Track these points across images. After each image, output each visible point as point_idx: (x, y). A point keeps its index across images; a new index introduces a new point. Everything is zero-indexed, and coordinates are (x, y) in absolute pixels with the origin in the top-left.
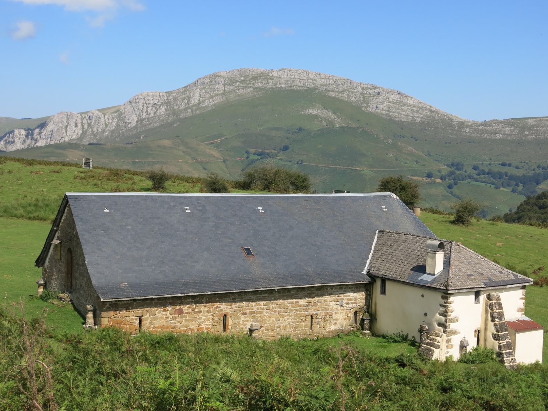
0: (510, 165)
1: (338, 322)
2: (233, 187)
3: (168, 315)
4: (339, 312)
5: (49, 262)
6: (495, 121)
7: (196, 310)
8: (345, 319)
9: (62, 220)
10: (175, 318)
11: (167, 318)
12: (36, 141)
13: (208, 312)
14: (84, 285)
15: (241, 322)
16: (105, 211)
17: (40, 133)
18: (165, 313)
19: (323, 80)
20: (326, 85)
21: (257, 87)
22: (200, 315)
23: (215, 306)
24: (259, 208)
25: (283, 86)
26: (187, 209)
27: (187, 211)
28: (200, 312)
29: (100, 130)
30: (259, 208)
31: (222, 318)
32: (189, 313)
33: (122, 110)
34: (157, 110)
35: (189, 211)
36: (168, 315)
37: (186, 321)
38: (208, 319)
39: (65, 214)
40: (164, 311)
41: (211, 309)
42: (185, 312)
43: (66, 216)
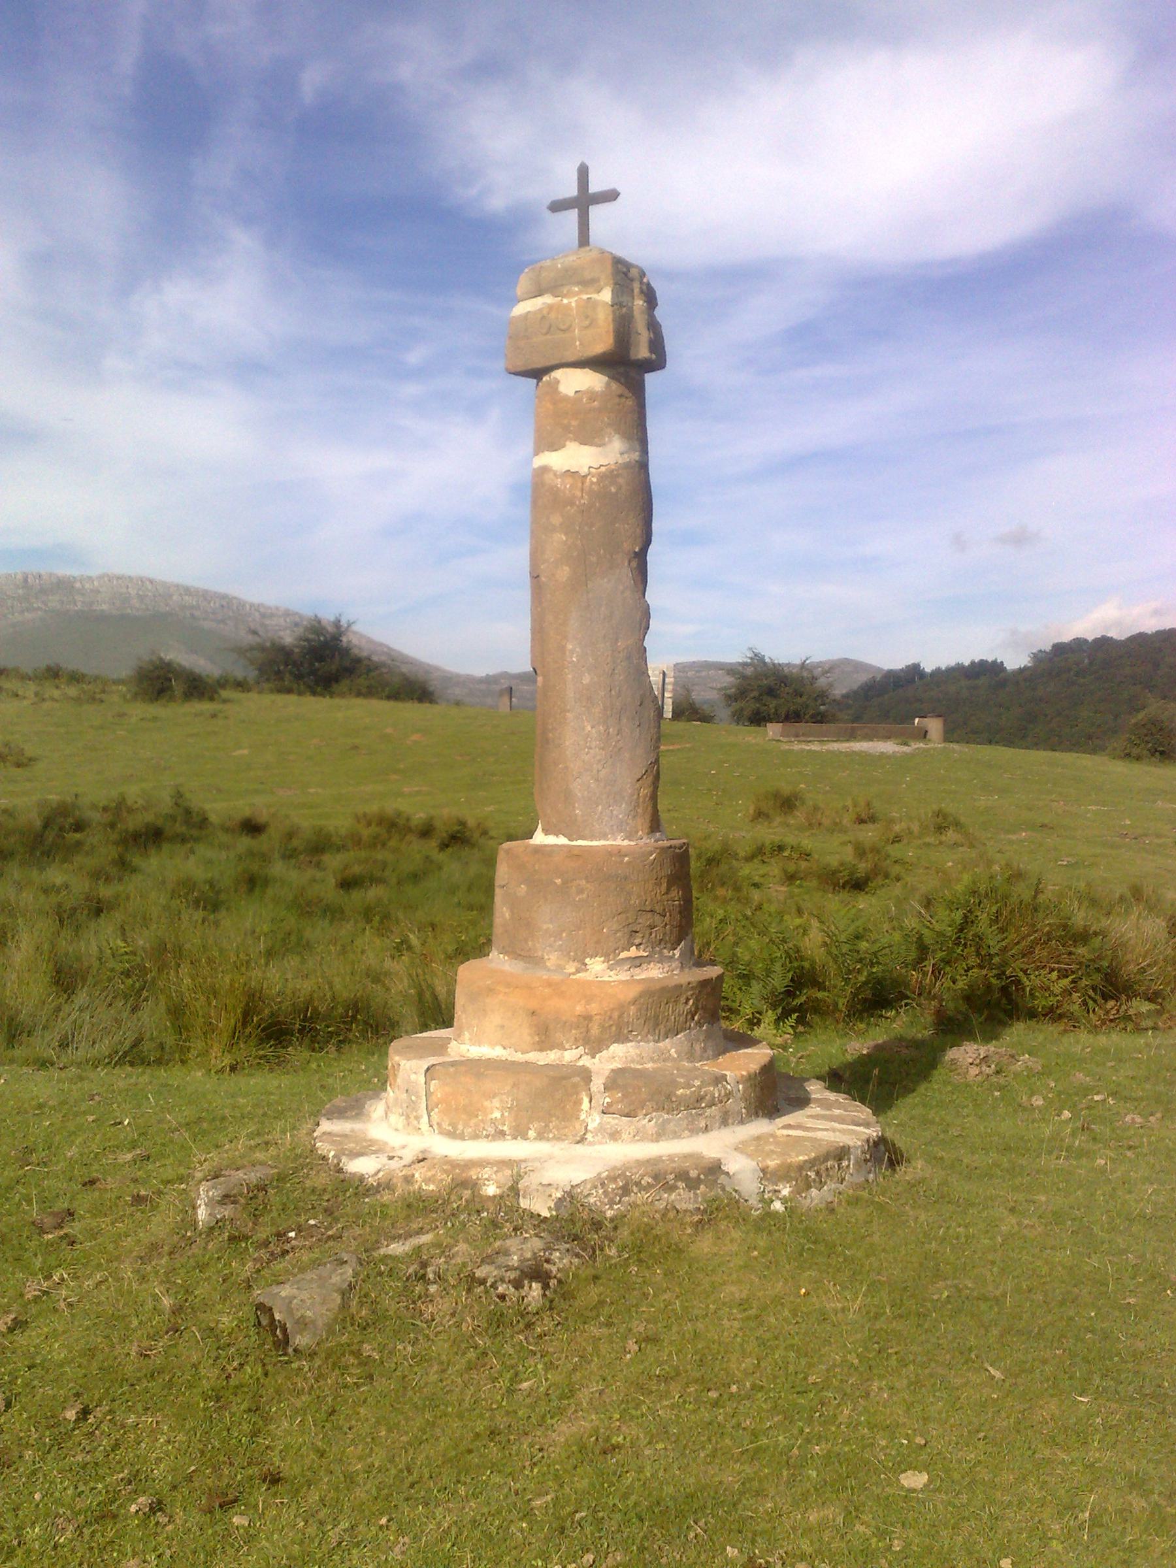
20: (192, 607)
25: (104, 607)
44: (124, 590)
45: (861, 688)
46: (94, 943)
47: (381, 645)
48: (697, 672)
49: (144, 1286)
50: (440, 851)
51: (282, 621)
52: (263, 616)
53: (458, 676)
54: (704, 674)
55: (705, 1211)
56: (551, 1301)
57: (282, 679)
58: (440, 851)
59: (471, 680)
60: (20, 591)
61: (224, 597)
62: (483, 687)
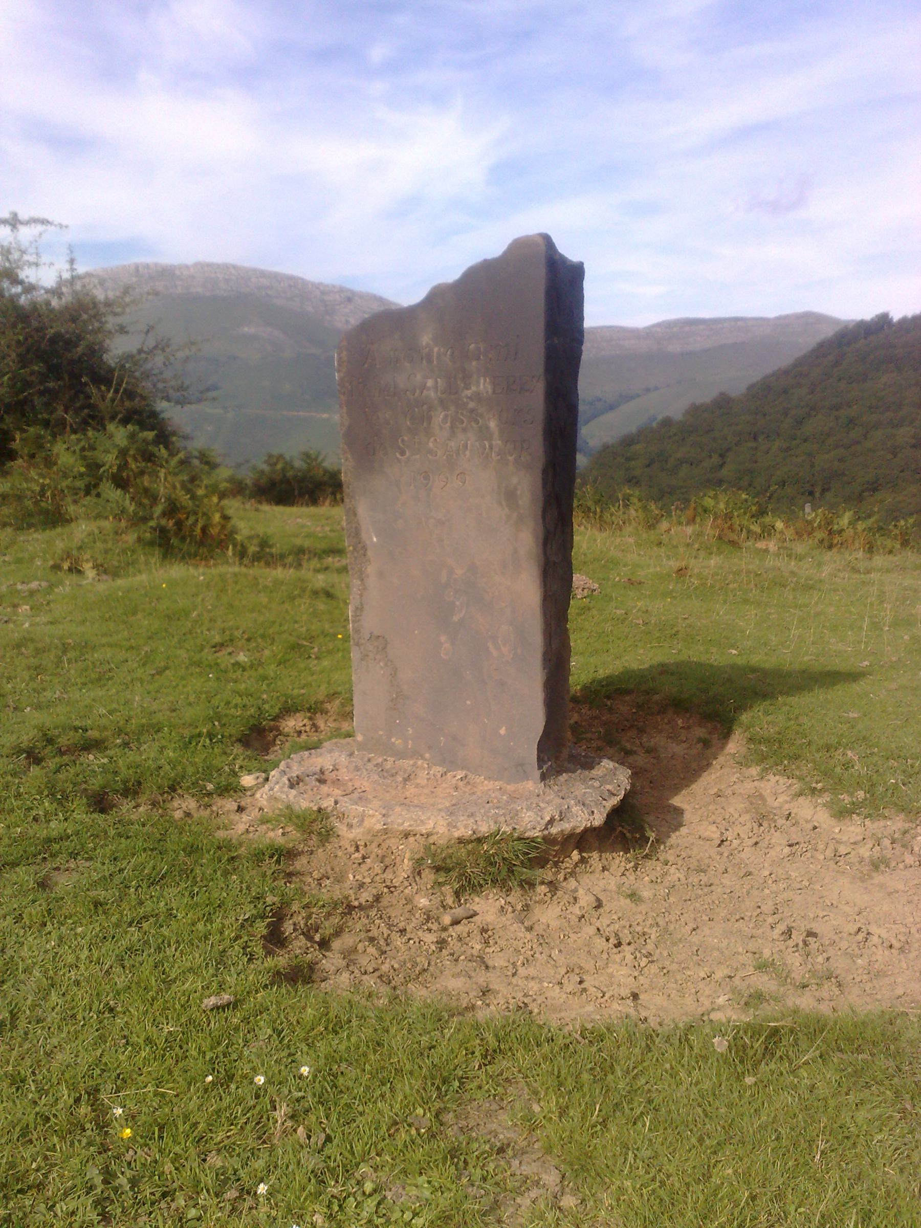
25: (200, 290)
52: (323, 293)
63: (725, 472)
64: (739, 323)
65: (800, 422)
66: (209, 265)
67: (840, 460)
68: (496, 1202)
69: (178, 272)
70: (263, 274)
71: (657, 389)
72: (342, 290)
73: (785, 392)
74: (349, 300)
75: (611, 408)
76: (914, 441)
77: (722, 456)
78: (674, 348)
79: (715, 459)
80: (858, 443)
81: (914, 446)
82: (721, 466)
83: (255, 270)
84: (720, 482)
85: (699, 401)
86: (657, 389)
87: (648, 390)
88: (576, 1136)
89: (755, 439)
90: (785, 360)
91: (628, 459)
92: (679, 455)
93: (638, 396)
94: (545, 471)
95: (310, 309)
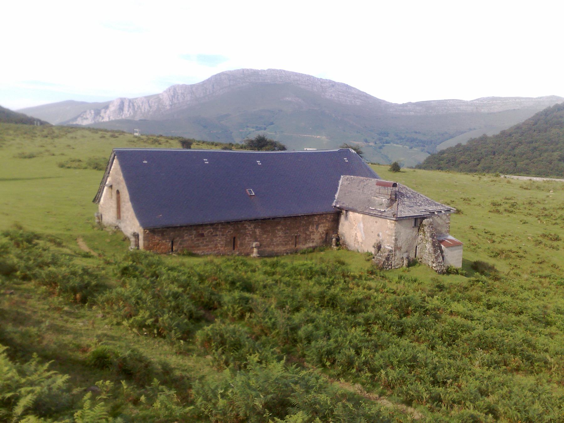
0: (419, 133)
1: (315, 241)
2: (42, 299)
3: (193, 238)
4: (315, 234)
5: (103, 200)
6: (410, 103)
7: (214, 234)
8: (319, 239)
9: (112, 169)
10: (198, 240)
11: (192, 240)
12: (103, 118)
13: (223, 235)
14: (129, 217)
15: (246, 242)
16: (144, 162)
17: (105, 112)
18: (191, 236)
19: (296, 77)
20: (297, 80)
21: (66, 412)
22: (217, 238)
23: (227, 231)
24: (258, 162)
25: (269, 81)
26: (206, 161)
27: (205, 163)
28: (217, 235)
29: (146, 110)
30: (258, 162)
31: (232, 240)
32: (209, 236)
33: (161, 97)
34: (185, 97)
35: (207, 163)
36: (193, 238)
37: (206, 242)
38: (222, 240)
39: (114, 165)
40: (190, 235)
41: (225, 233)
42: (205, 235)
43: (115, 166)
44: (275, 75)
45: (544, 110)
46: (281, 248)
47: (363, 92)
48: (488, 101)
49: (246, 402)
50: (390, 170)
51: (328, 85)
52: (322, 83)
53: (392, 104)
54: (490, 102)
55: (310, 236)
56: (370, 335)
57: (139, 272)
58: (390, 170)
59: (396, 105)
60: (242, 76)
61: (309, 76)
62: (400, 108)
63: (479, 167)
64: (517, 100)
65: (513, 148)
66: (274, 70)
67: (527, 164)
68: (333, 281)
69: (260, 73)
70: (296, 74)
71: (475, 129)
72: (330, 81)
73: (510, 135)
74: (333, 86)
75: (452, 137)
76: (559, 158)
77: (479, 160)
78: (484, 110)
79: (476, 162)
80: (536, 158)
81: (560, 160)
82: (478, 165)
83: (293, 73)
84: (476, 171)
85: (473, 137)
86: (475, 129)
87: (470, 129)
88: (370, 343)
89: (494, 154)
90: (508, 124)
91: (440, 160)
92: (461, 159)
93: (465, 132)
94: (24, 115)
95: (315, 90)
